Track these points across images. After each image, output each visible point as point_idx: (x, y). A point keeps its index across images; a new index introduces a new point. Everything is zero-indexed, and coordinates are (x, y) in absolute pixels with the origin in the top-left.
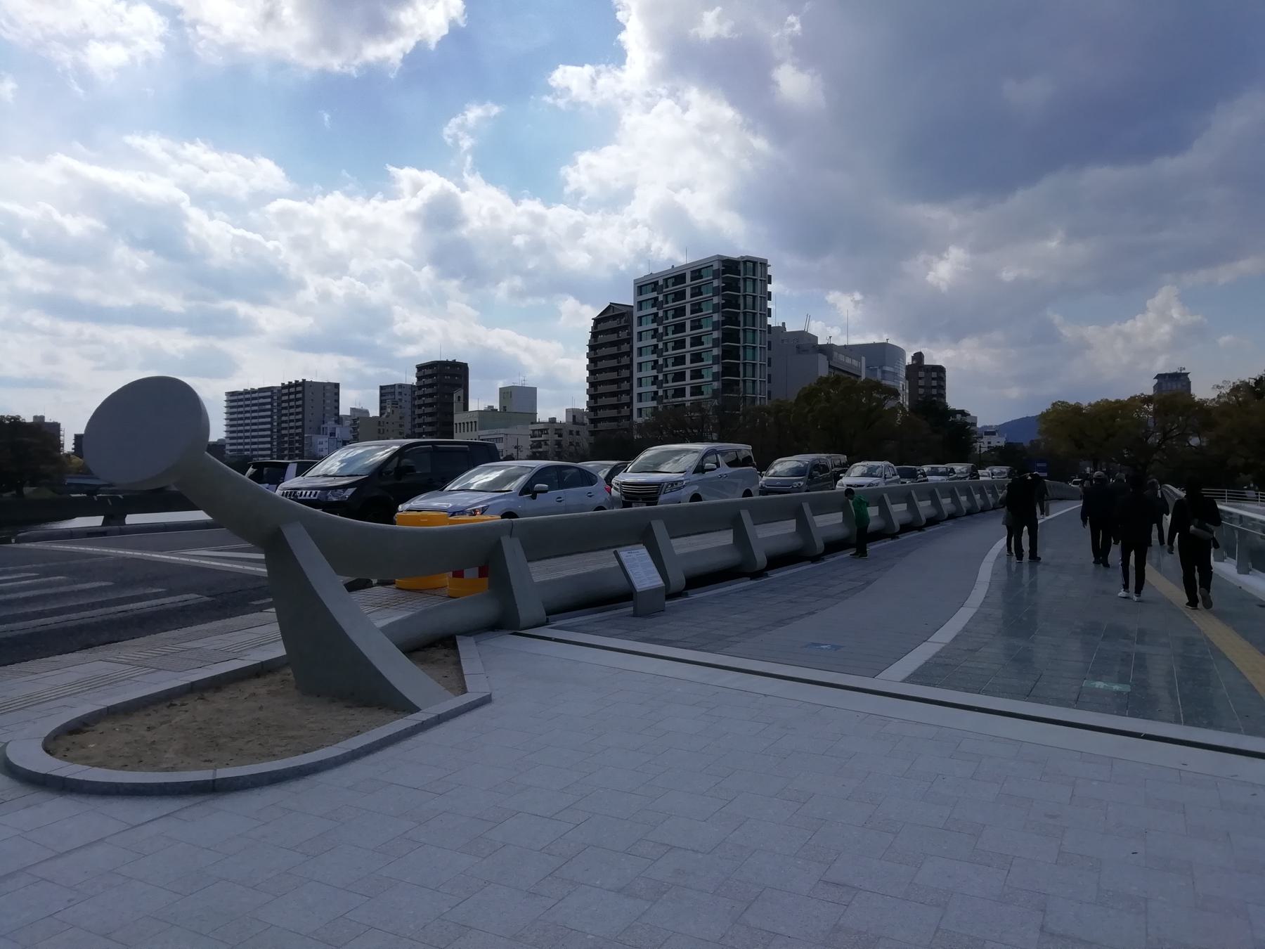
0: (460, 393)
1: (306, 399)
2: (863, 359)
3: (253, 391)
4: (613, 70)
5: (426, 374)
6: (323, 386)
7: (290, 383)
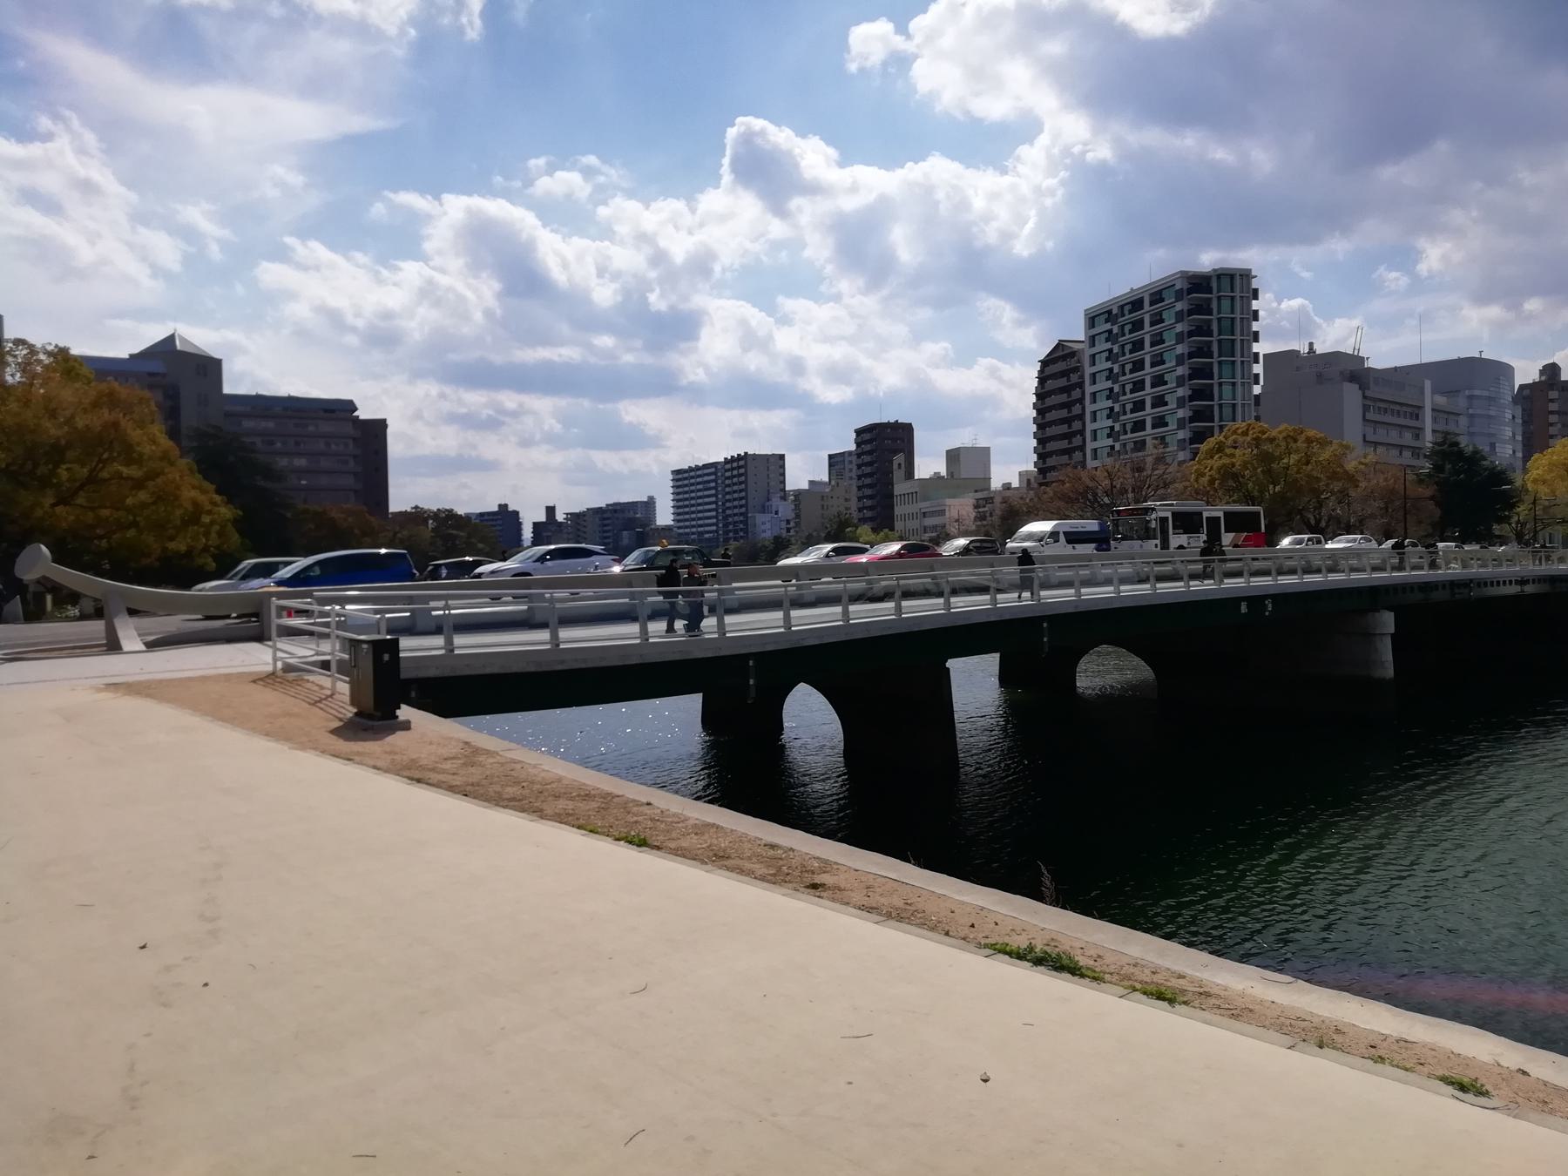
1: (748, 473)
3: (698, 468)
6: (767, 458)
7: (732, 457)
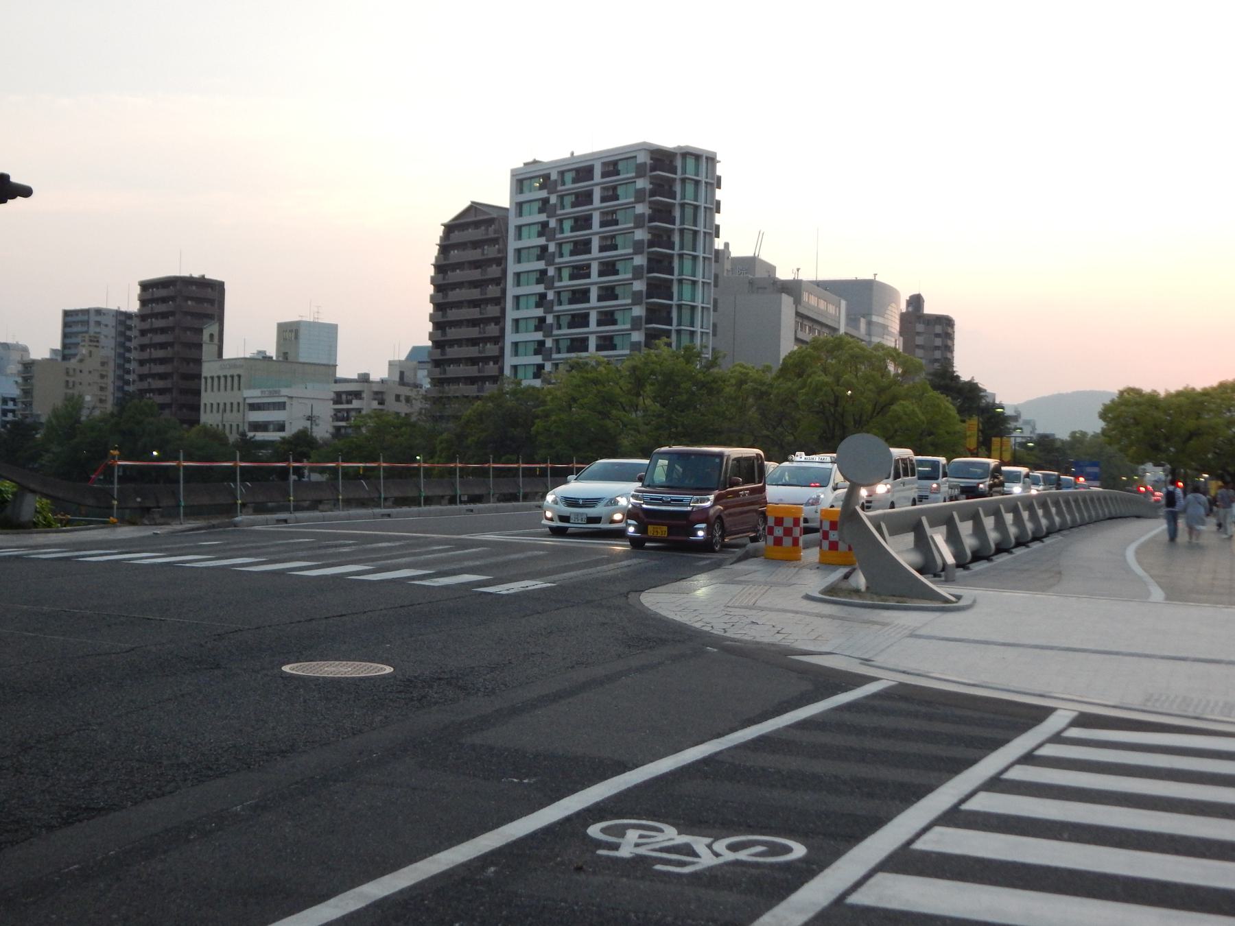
0: (214, 329)
2: (843, 303)
5: (156, 310)
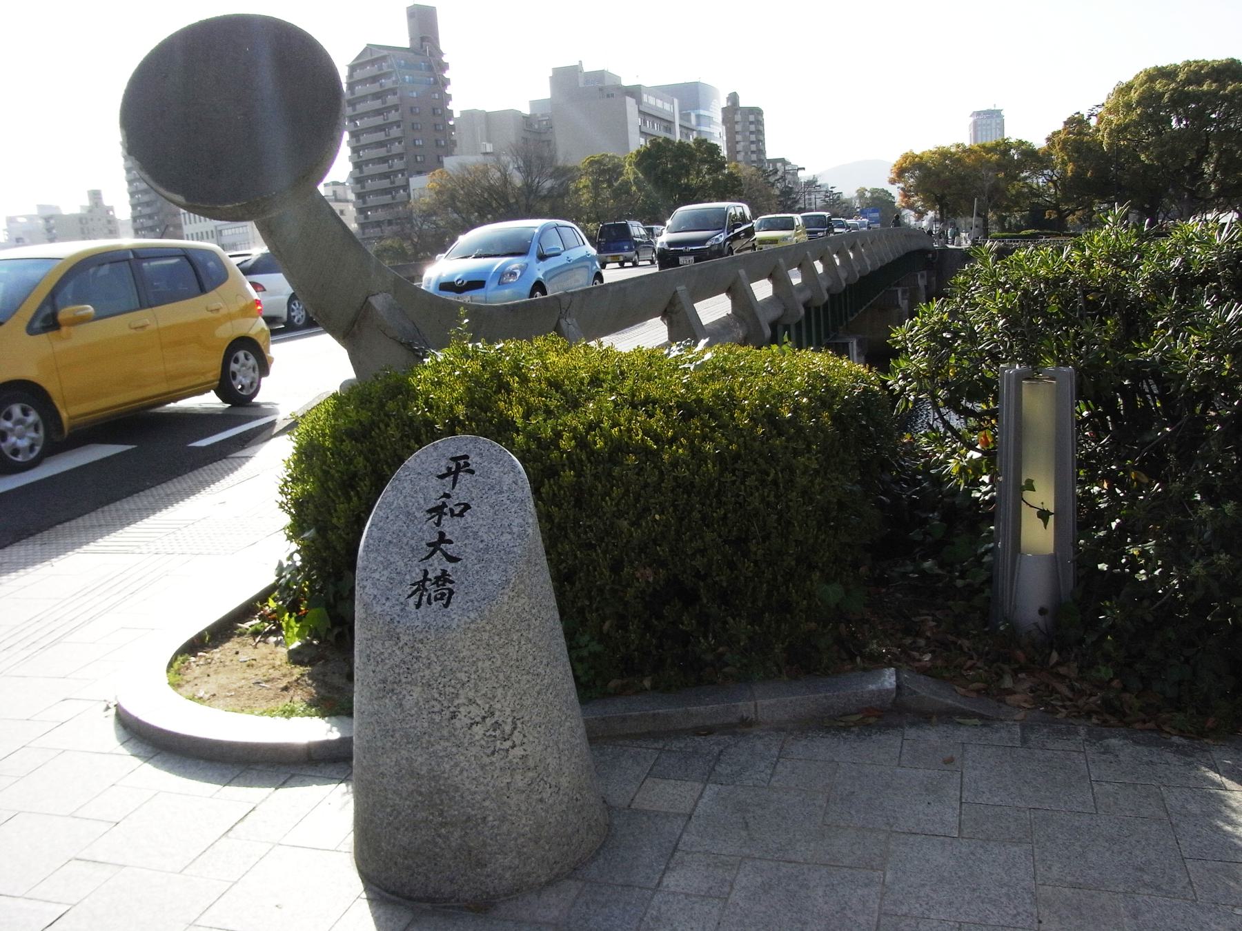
2: (676, 101)
4: (299, 489)
